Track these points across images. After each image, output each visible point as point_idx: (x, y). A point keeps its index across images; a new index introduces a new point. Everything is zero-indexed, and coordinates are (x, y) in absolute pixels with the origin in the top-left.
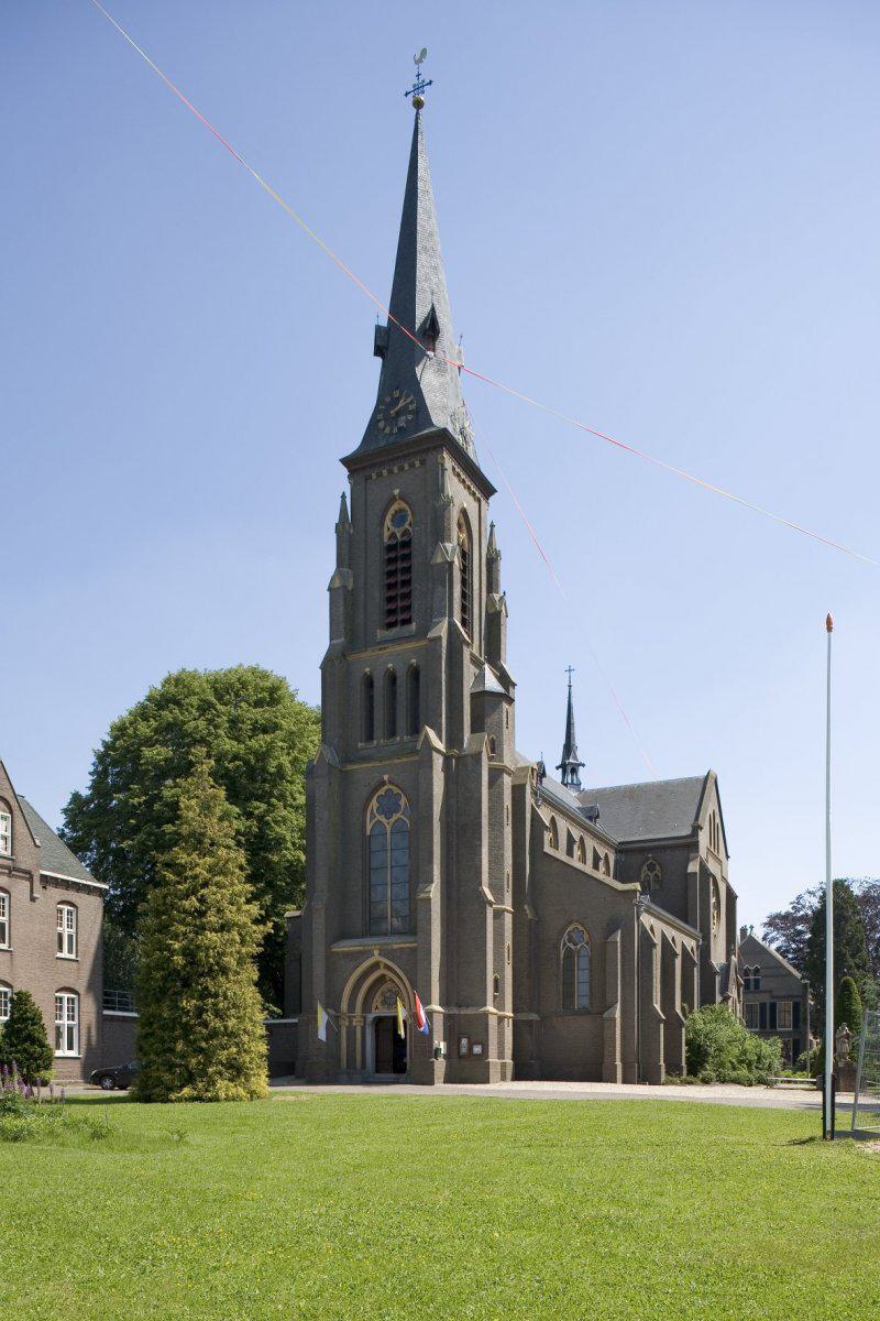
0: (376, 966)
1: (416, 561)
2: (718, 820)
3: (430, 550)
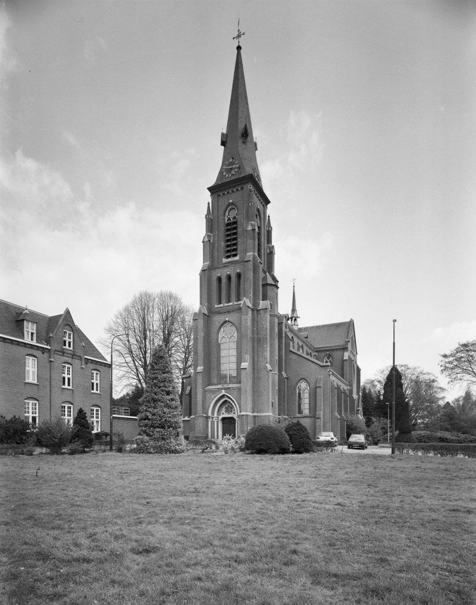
0: (223, 396)
1: (239, 230)
2: (354, 339)
3: (245, 225)
